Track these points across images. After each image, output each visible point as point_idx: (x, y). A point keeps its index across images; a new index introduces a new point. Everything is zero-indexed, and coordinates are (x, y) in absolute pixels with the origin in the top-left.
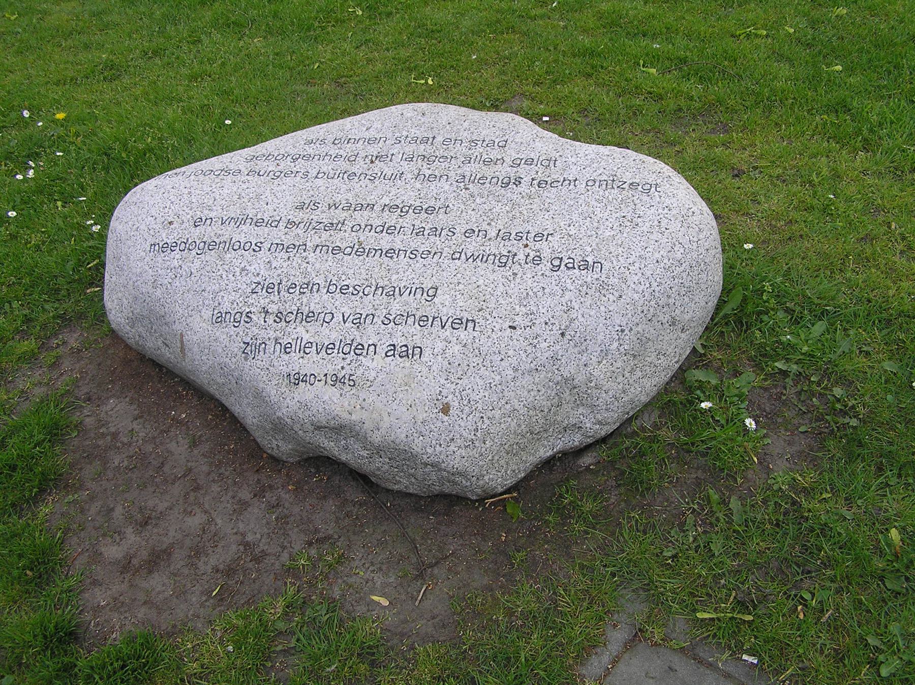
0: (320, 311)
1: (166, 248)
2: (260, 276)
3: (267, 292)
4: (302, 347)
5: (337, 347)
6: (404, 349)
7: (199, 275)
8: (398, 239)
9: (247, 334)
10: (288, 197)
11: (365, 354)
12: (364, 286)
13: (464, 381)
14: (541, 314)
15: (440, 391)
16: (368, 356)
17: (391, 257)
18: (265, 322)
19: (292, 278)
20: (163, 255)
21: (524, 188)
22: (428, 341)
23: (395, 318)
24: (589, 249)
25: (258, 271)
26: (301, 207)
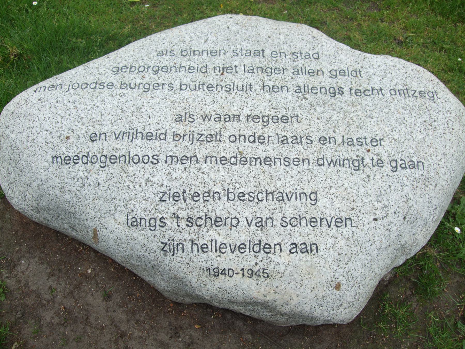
0: (226, 216)
1: (67, 160)
2: (165, 186)
3: (174, 200)
4: (218, 248)
5: (248, 247)
6: (304, 246)
7: (107, 185)
8: (270, 147)
9: (164, 236)
10: (165, 110)
11: (273, 251)
12: (257, 193)
13: (350, 265)
14: (392, 207)
15: (334, 275)
16: (276, 254)
17: (270, 165)
18: (179, 226)
19: (193, 187)
20: (67, 167)
21: (346, 97)
22: (321, 239)
23: (290, 221)
24: (412, 151)
25: (161, 182)
26: (179, 119)
